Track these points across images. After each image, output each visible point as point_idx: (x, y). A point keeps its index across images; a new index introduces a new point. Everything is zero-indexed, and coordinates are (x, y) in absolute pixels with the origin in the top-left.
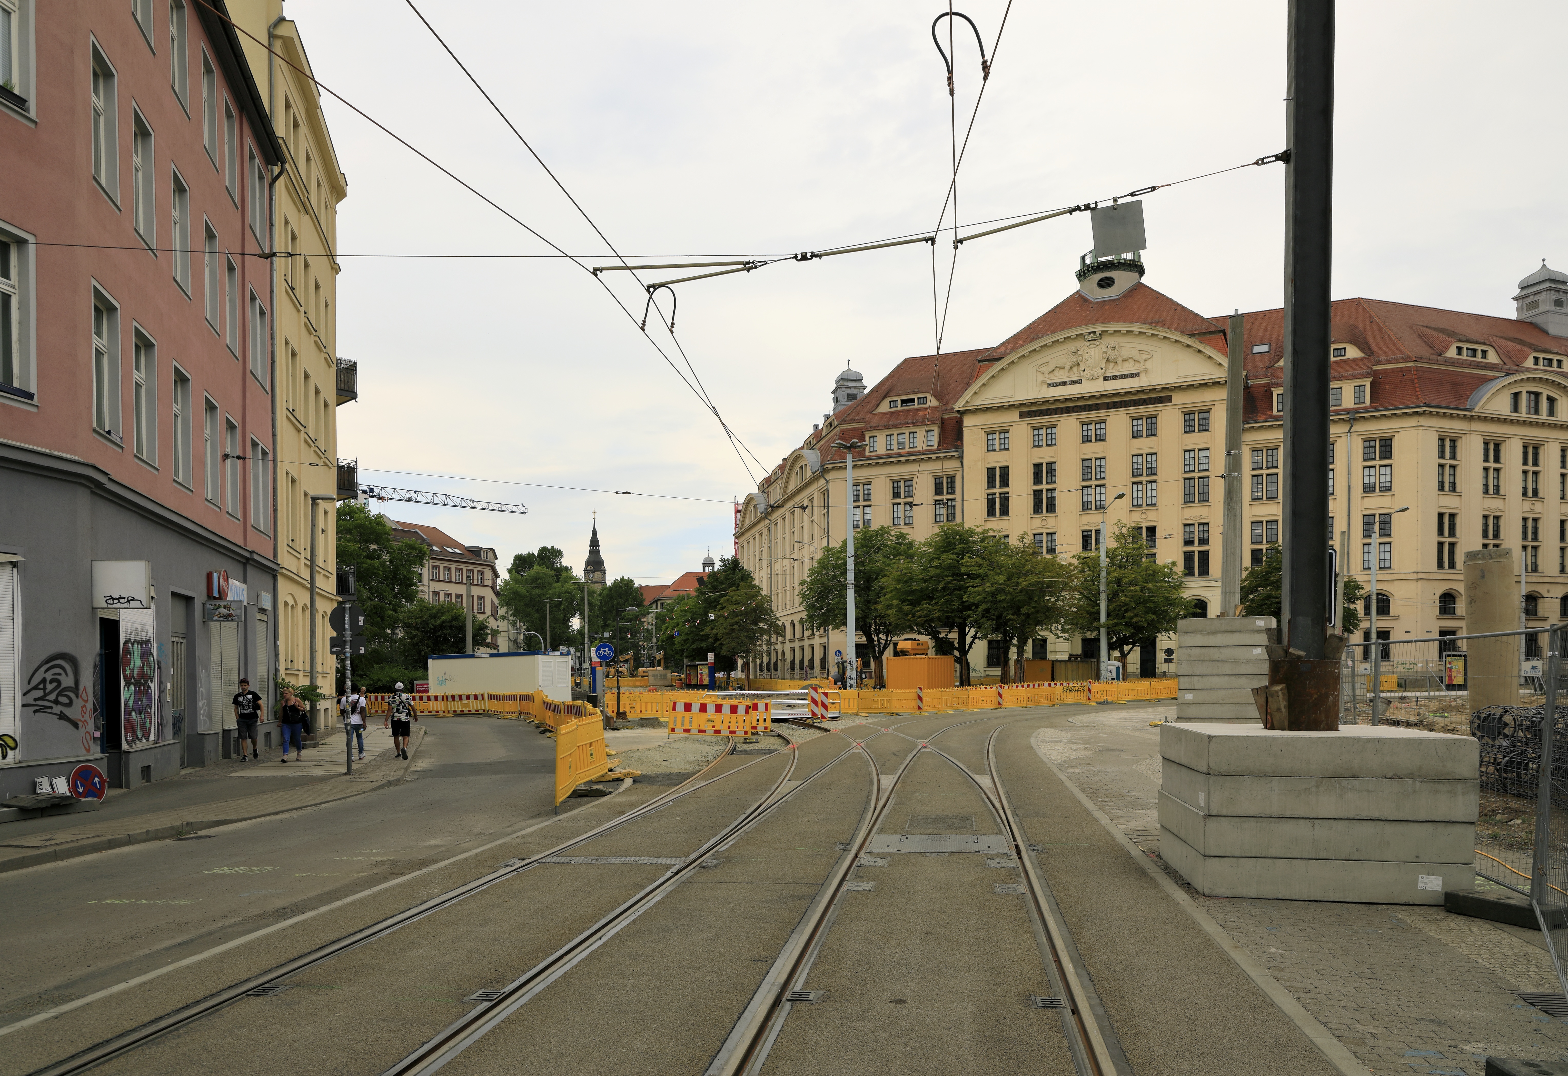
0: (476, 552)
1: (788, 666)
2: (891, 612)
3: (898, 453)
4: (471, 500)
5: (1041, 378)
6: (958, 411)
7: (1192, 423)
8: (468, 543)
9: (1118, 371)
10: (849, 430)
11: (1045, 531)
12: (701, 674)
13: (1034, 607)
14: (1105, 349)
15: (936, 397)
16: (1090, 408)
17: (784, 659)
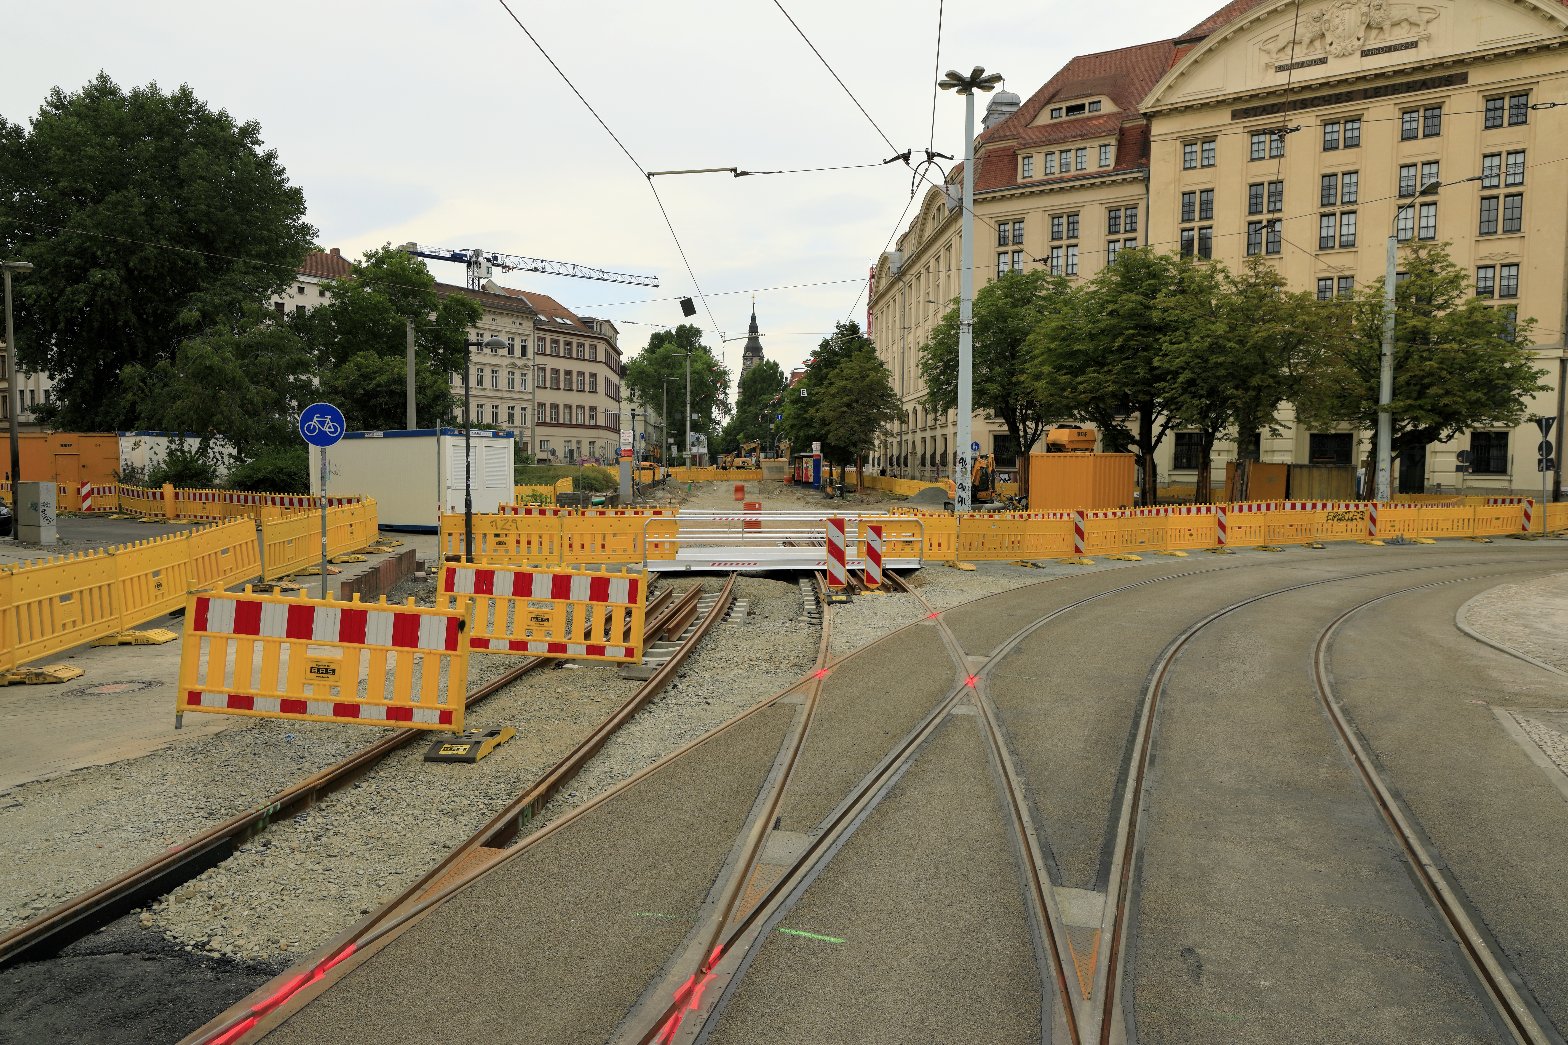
0: (589, 323)
1: (918, 462)
2: (1041, 384)
3: (1061, 178)
4: (600, 271)
5: (1265, 59)
6: (1144, 114)
7: (1498, 113)
8: (582, 313)
9: (1384, 40)
10: (996, 151)
12: (807, 468)
14: (1365, 9)
15: (1115, 100)
16: (1338, 99)
17: (914, 453)
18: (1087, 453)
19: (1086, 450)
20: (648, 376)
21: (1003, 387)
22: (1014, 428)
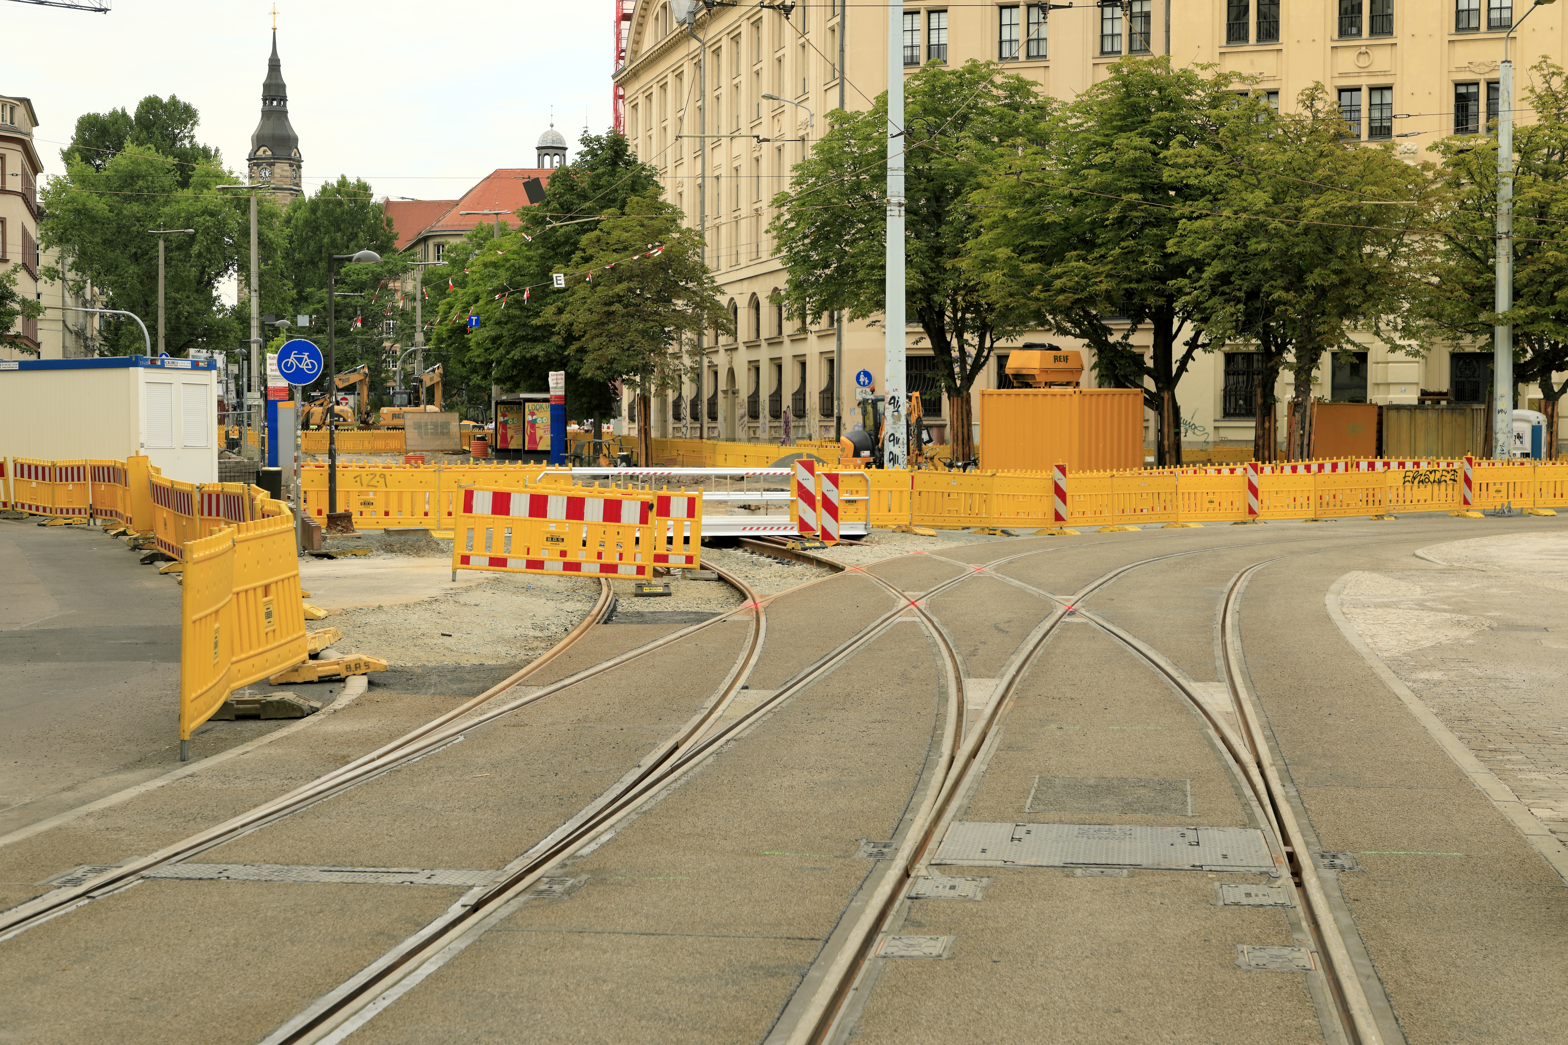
2: (993, 277)
11: (1364, 82)
13: (1337, 272)
18: (1070, 389)
19: (1068, 384)
20: (94, 220)
21: (924, 274)
22: (942, 346)
